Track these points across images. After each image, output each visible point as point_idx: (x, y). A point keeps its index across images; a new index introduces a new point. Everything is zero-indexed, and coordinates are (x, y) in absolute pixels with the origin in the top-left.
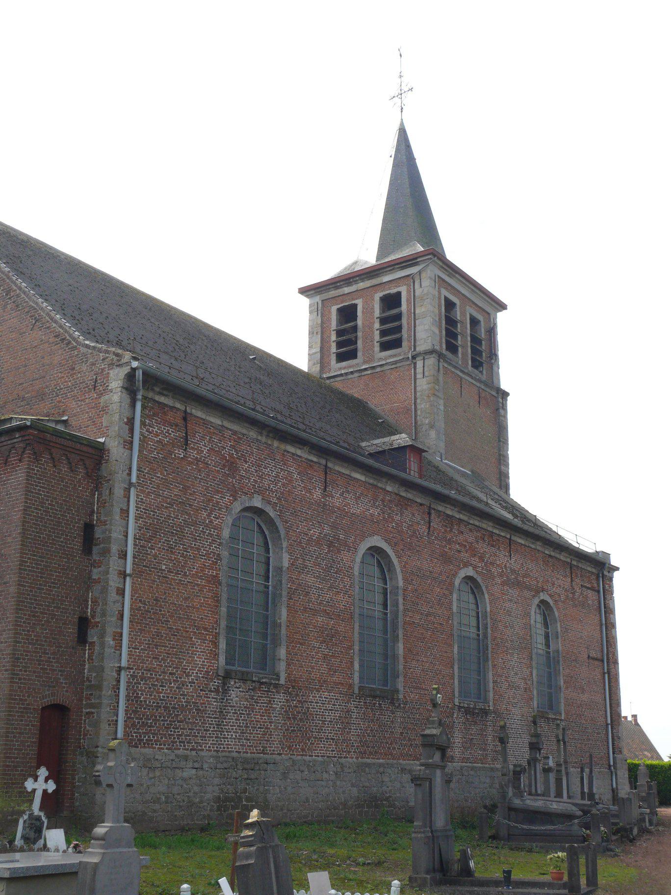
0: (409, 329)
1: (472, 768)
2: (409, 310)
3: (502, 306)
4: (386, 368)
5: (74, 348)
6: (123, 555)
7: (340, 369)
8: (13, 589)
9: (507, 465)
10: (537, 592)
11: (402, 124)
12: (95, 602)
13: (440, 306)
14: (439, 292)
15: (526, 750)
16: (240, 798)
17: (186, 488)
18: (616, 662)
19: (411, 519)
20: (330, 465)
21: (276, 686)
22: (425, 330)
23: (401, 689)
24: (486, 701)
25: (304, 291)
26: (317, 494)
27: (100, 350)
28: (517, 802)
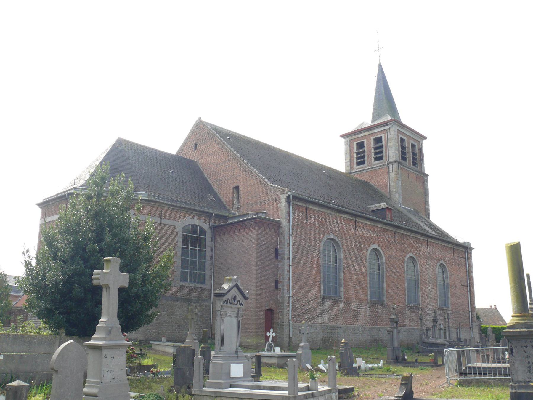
0: (386, 152)
1: (413, 329)
2: (386, 144)
3: (425, 138)
4: (377, 168)
5: (267, 186)
6: (289, 259)
7: (358, 168)
8: (255, 272)
9: (429, 205)
10: (439, 260)
11: (380, 63)
12: (280, 275)
13: (398, 142)
14: (398, 136)
15: (432, 323)
16: (329, 340)
17: (307, 234)
18: (473, 287)
19: (388, 236)
20: (357, 220)
21: (340, 301)
22: (392, 152)
23: (385, 300)
24: (418, 304)
25: (342, 136)
26: (353, 231)
27: (277, 188)
28: (426, 340)
